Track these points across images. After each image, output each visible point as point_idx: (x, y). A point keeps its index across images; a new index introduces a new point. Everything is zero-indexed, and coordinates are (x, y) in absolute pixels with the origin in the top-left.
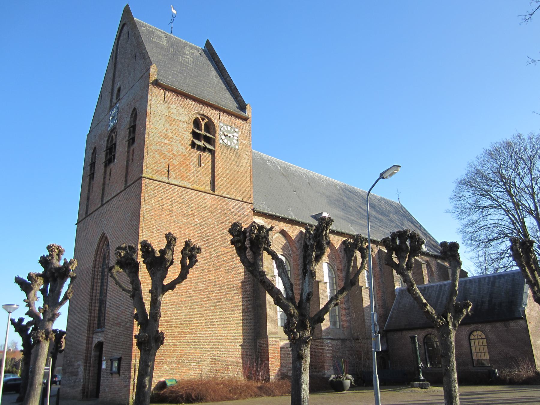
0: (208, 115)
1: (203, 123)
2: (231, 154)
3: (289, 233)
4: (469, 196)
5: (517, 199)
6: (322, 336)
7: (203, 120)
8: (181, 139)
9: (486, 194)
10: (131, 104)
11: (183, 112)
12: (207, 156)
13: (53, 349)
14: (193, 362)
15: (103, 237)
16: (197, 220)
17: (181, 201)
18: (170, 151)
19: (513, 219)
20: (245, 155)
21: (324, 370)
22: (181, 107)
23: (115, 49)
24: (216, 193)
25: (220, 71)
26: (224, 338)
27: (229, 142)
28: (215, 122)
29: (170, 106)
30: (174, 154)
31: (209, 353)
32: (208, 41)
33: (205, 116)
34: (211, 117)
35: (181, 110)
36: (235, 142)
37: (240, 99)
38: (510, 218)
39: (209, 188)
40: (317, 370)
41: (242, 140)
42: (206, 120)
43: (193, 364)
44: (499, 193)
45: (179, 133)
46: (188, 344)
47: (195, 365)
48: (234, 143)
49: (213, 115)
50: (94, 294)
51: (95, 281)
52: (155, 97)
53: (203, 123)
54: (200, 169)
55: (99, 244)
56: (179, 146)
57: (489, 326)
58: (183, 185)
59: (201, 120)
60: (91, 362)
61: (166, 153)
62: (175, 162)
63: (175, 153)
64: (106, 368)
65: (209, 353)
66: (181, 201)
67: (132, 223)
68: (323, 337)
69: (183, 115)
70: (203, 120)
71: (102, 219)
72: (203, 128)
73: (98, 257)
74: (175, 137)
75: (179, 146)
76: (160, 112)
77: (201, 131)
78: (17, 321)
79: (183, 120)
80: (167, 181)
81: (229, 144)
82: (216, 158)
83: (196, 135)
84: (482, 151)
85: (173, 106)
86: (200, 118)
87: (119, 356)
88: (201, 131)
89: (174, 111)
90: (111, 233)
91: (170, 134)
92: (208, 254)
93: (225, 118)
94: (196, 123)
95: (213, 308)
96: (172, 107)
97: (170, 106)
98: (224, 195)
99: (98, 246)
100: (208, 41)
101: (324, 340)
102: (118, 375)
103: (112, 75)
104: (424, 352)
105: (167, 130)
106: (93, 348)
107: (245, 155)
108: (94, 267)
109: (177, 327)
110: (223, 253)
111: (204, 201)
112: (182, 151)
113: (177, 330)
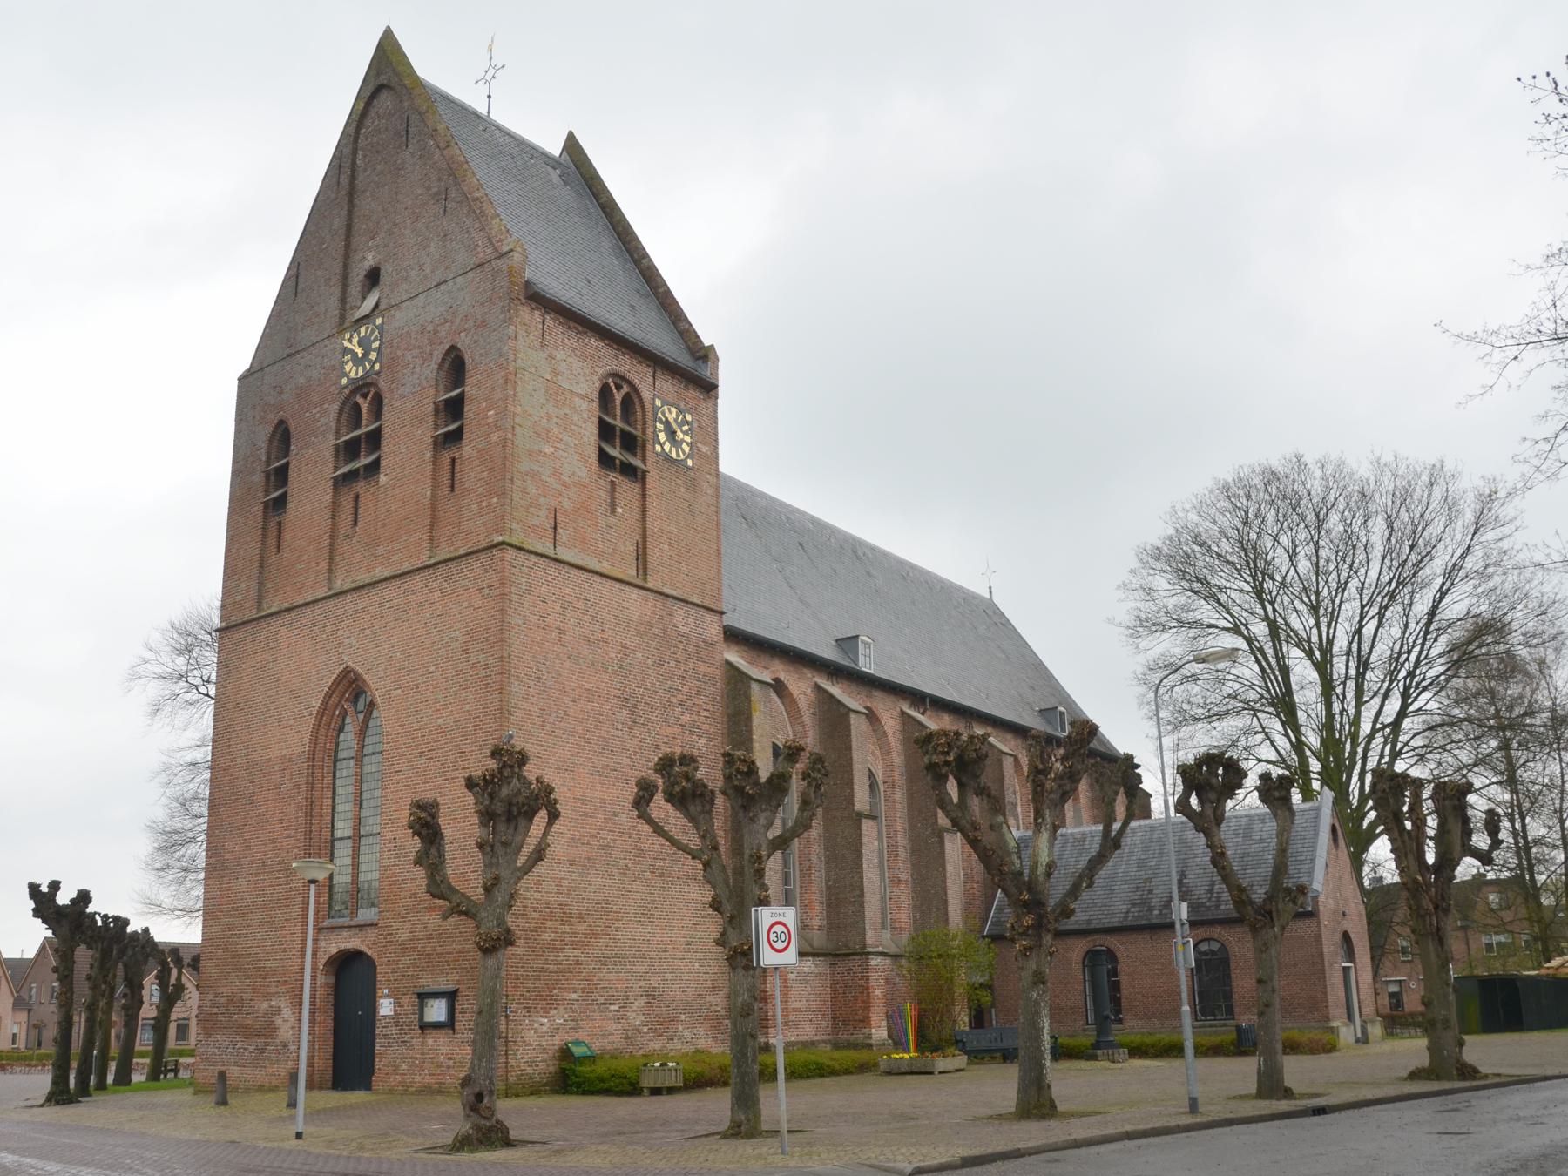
0: (630, 376)
1: (618, 398)
2: (679, 482)
3: (790, 687)
4: (1169, 592)
5: (1274, 610)
6: (864, 946)
7: (618, 387)
8: (577, 442)
9: (1211, 594)
10: (436, 332)
11: (580, 371)
12: (627, 489)
13: (92, 966)
14: (614, 1004)
15: (342, 680)
16: (613, 655)
17: (581, 604)
18: (556, 474)
19: (1264, 663)
20: (705, 485)
21: (869, 1025)
22: (576, 355)
23: (347, 150)
24: (650, 585)
25: (618, 234)
26: (670, 948)
27: (674, 449)
28: (646, 394)
29: (555, 353)
30: (565, 484)
31: (642, 983)
32: (571, 137)
33: (623, 378)
34: (636, 382)
35: (577, 364)
36: (687, 449)
37: (687, 326)
38: (1258, 661)
39: (630, 573)
40: (848, 1028)
41: (699, 445)
42: (625, 389)
43: (613, 1008)
44: (1237, 589)
45: (573, 427)
46: (603, 961)
47: (617, 1011)
48: (684, 453)
49: (641, 376)
50: (315, 829)
51: (317, 793)
52: (524, 328)
53: (618, 398)
54: (612, 520)
55: (328, 696)
56: (575, 462)
57: (1238, 929)
58: (580, 563)
59: (615, 391)
60: (318, 1000)
61: (548, 480)
62: (567, 504)
63: (567, 479)
64: (396, 1013)
65: (642, 983)
66: (581, 604)
67: (472, 659)
68: (871, 950)
69: (582, 379)
70: (618, 387)
71: (340, 632)
72: (618, 412)
73: (322, 731)
74: (566, 438)
75: (575, 462)
76: (533, 370)
77: (615, 419)
78: (44, 889)
79: (580, 391)
80: (551, 553)
81: (674, 455)
82: (649, 492)
83: (606, 431)
84: (1210, 484)
85: (560, 355)
86: (612, 384)
87: (451, 988)
88: (615, 419)
89: (562, 367)
90: (382, 674)
91: (556, 430)
92: (636, 741)
93: (667, 385)
94: (605, 394)
95: (648, 874)
96: (558, 357)
97: (555, 353)
98: (665, 590)
99: (325, 703)
100: (571, 137)
101: (871, 957)
102: (451, 1032)
103: (338, 223)
104: (1082, 988)
105: (549, 418)
106: (321, 967)
107: (705, 485)
108: (312, 755)
109: (581, 919)
110: (666, 740)
111: (626, 604)
112: (580, 474)
113: (581, 927)
